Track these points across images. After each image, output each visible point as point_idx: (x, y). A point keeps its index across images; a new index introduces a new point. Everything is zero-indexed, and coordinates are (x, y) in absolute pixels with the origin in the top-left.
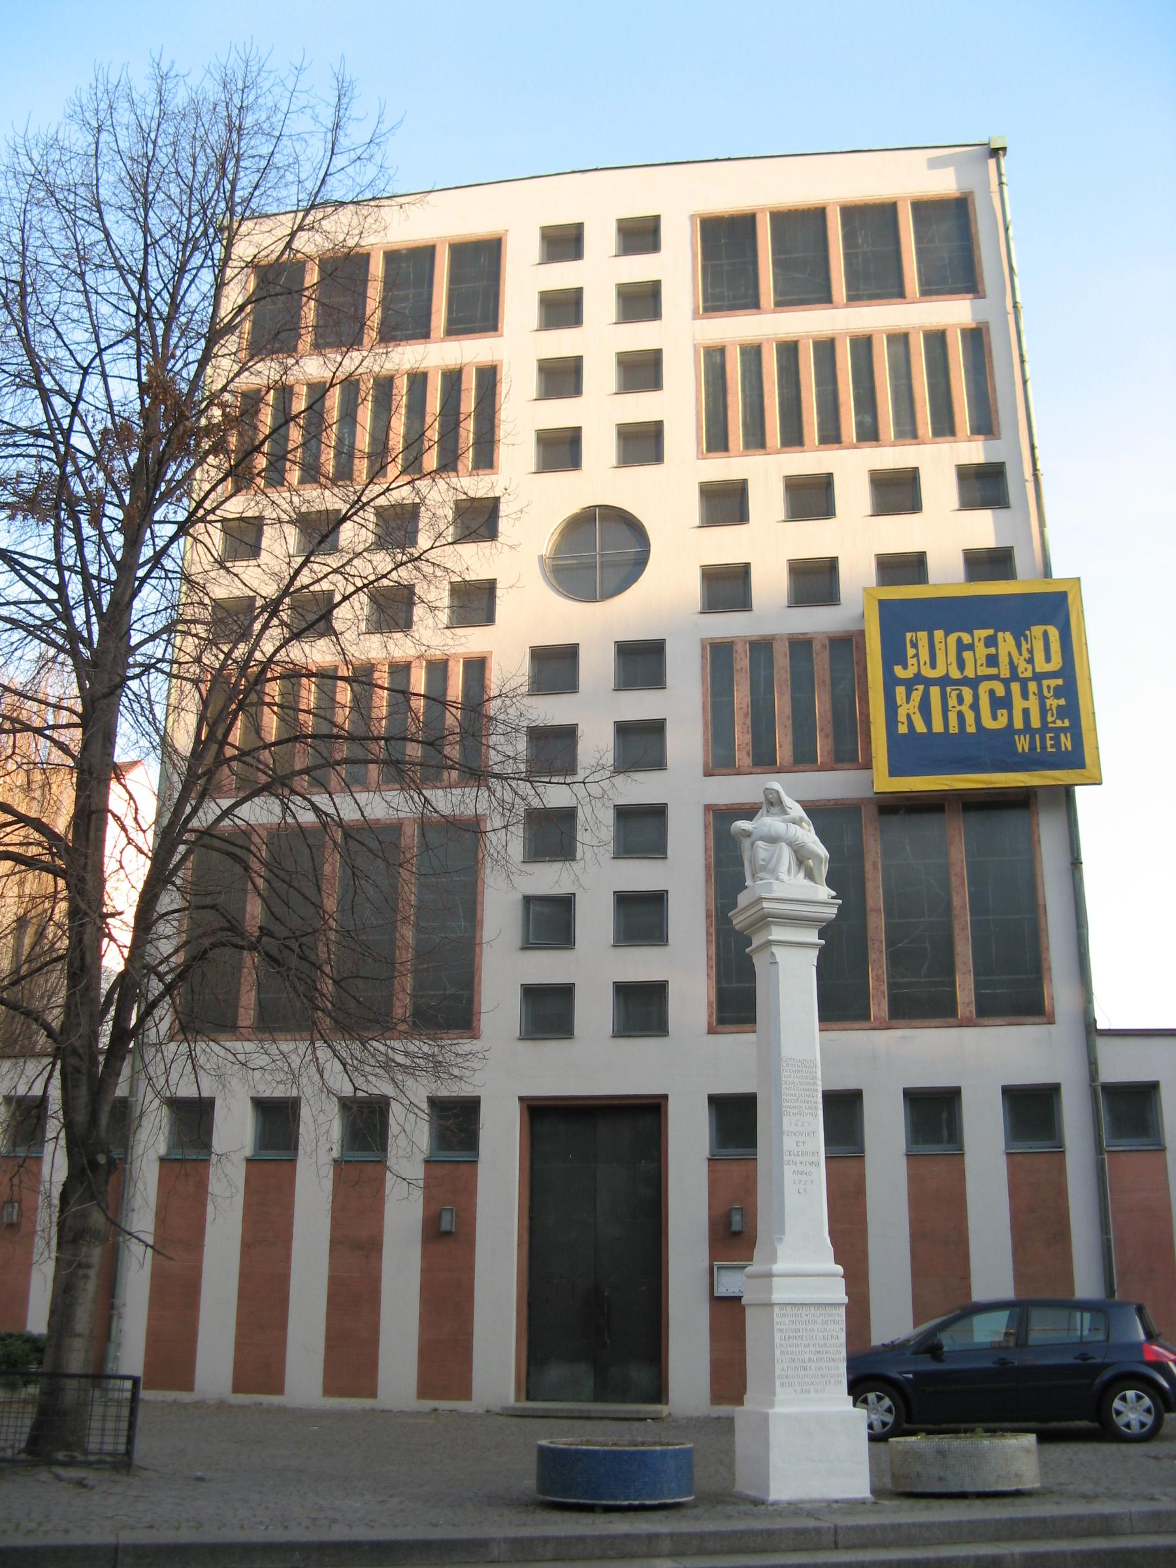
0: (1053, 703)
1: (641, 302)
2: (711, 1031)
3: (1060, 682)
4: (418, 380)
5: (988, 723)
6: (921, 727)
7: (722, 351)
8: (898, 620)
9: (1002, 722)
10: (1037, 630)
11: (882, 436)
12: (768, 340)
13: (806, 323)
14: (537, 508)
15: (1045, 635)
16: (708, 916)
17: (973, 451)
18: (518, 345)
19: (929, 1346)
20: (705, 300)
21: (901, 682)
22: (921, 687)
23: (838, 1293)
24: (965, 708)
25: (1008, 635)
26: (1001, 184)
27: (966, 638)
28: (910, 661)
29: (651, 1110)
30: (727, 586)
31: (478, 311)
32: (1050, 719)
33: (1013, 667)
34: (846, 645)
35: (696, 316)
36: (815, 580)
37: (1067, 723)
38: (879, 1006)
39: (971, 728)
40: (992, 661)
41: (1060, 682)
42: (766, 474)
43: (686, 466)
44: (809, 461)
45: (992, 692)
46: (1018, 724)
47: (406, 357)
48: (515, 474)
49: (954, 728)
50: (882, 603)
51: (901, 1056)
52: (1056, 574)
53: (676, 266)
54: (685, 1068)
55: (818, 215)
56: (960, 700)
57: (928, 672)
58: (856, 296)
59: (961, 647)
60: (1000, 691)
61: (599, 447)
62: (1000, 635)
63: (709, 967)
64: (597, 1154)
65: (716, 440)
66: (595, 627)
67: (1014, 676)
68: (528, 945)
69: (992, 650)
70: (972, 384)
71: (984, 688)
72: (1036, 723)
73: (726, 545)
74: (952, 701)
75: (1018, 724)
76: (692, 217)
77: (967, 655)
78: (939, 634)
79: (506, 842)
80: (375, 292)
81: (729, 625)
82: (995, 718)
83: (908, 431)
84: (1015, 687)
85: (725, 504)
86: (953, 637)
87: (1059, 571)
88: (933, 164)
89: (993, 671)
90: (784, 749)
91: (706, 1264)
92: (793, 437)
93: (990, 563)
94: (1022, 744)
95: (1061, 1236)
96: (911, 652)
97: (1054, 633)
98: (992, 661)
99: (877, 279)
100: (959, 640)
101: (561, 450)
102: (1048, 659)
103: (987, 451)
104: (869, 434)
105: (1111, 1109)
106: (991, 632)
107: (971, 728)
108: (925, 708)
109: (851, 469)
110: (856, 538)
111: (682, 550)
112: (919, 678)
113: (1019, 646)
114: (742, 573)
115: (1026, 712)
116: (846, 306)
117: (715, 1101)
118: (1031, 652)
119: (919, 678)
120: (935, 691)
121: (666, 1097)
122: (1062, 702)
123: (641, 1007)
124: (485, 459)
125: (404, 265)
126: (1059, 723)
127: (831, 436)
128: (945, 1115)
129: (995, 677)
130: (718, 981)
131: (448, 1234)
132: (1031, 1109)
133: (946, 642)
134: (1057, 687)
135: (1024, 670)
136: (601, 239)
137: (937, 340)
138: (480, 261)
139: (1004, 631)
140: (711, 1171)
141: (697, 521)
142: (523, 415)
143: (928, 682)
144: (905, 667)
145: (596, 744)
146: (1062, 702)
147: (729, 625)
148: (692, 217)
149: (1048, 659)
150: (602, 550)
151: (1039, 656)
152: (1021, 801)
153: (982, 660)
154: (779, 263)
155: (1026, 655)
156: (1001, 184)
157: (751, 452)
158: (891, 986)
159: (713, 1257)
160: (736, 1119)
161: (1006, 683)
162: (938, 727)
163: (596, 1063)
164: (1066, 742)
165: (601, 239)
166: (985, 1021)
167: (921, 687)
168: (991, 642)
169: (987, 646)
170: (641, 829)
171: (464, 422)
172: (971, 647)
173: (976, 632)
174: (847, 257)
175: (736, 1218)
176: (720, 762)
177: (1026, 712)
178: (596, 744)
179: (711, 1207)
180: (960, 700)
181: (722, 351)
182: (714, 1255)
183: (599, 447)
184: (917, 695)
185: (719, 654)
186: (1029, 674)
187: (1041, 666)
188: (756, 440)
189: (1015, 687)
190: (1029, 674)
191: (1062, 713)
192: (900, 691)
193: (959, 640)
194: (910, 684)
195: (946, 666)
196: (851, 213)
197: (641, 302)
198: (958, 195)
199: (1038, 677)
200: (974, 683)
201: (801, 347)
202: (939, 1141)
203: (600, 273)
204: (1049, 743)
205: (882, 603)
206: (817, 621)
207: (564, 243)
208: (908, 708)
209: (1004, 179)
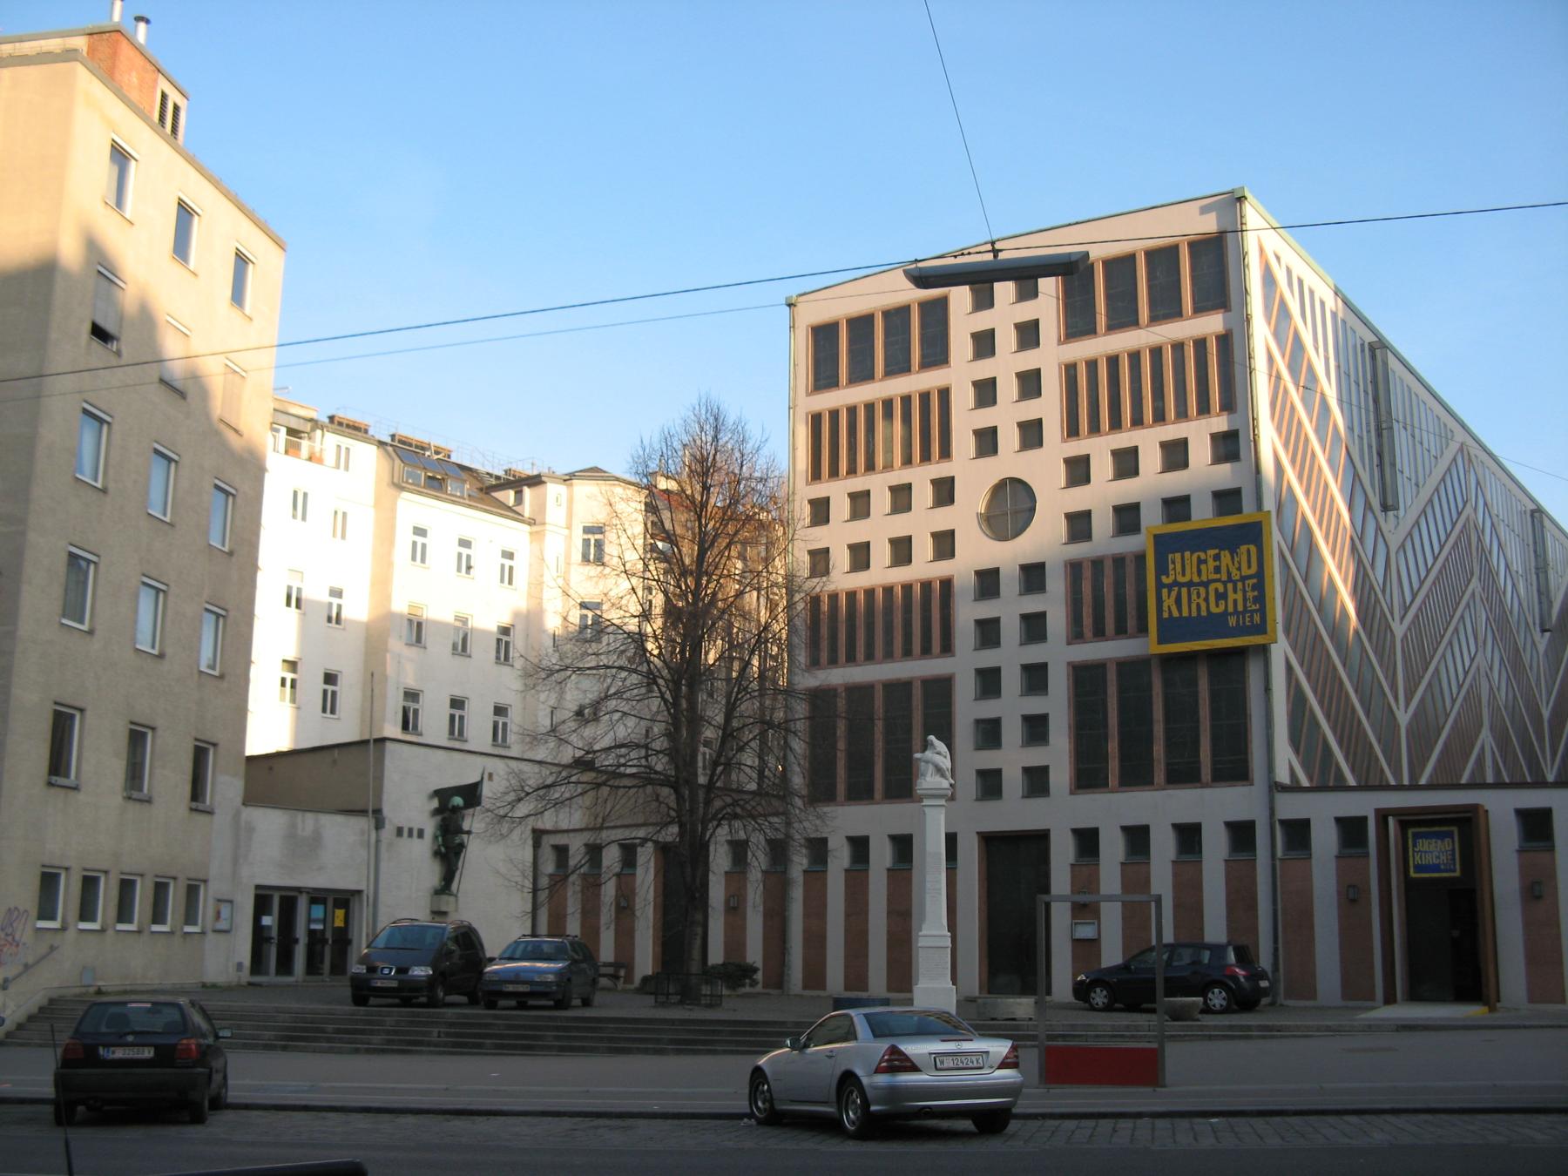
0: (1250, 595)
2: (1072, 793)
5: (1214, 609)
6: (1176, 614)
9: (1221, 609)
10: (1243, 548)
14: (975, 479)
17: (1220, 423)
19: (1125, 967)
20: (1067, 328)
21: (1164, 586)
27: (1203, 556)
29: (1039, 840)
30: (1079, 524)
33: (1229, 574)
36: (1127, 517)
38: (1160, 775)
39: (1204, 613)
40: (1217, 570)
42: (1100, 450)
43: (1056, 447)
46: (1231, 609)
48: (964, 465)
49: (1194, 614)
55: (1130, 258)
56: (1199, 595)
57: (1181, 579)
59: (1200, 562)
60: (1221, 590)
61: (1009, 438)
65: (1073, 431)
66: (1008, 555)
67: (1230, 579)
68: (979, 748)
71: (1212, 587)
72: (1240, 608)
74: (1194, 596)
75: (1231, 609)
77: (1203, 567)
78: (1187, 554)
81: (1081, 550)
84: (1230, 586)
85: (1078, 471)
88: (1204, 210)
93: (1227, 499)
94: (1232, 621)
98: (1217, 570)
103: (1229, 421)
107: (1204, 613)
108: (1178, 601)
109: (1149, 442)
111: (1054, 501)
115: (1235, 601)
119: (1176, 583)
120: (1184, 590)
123: (1037, 781)
124: (946, 453)
132: (1241, 834)
133: (1191, 558)
135: (1236, 575)
142: (965, 419)
143: (1181, 585)
150: (1011, 506)
152: (1241, 653)
153: (1211, 569)
154: (1108, 297)
161: (1225, 583)
162: (1185, 613)
168: (1217, 558)
170: (1035, 677)
171: (928, 427)
172: (1205, 562)
176: (1076, 635)
177: (1235, 601)
180: (1199, 595)
182: (1074, 917)
183: (1009, 438)
185: (1074, 568)
187: (1245, 572)
189: (1230, 586)
192: (1165, 591)
194: (1170, 587)
195: (1190, 575)
199: (1244, 579)
200: (1206, 585)
206: (1129, 544)
208: (1168, 602)
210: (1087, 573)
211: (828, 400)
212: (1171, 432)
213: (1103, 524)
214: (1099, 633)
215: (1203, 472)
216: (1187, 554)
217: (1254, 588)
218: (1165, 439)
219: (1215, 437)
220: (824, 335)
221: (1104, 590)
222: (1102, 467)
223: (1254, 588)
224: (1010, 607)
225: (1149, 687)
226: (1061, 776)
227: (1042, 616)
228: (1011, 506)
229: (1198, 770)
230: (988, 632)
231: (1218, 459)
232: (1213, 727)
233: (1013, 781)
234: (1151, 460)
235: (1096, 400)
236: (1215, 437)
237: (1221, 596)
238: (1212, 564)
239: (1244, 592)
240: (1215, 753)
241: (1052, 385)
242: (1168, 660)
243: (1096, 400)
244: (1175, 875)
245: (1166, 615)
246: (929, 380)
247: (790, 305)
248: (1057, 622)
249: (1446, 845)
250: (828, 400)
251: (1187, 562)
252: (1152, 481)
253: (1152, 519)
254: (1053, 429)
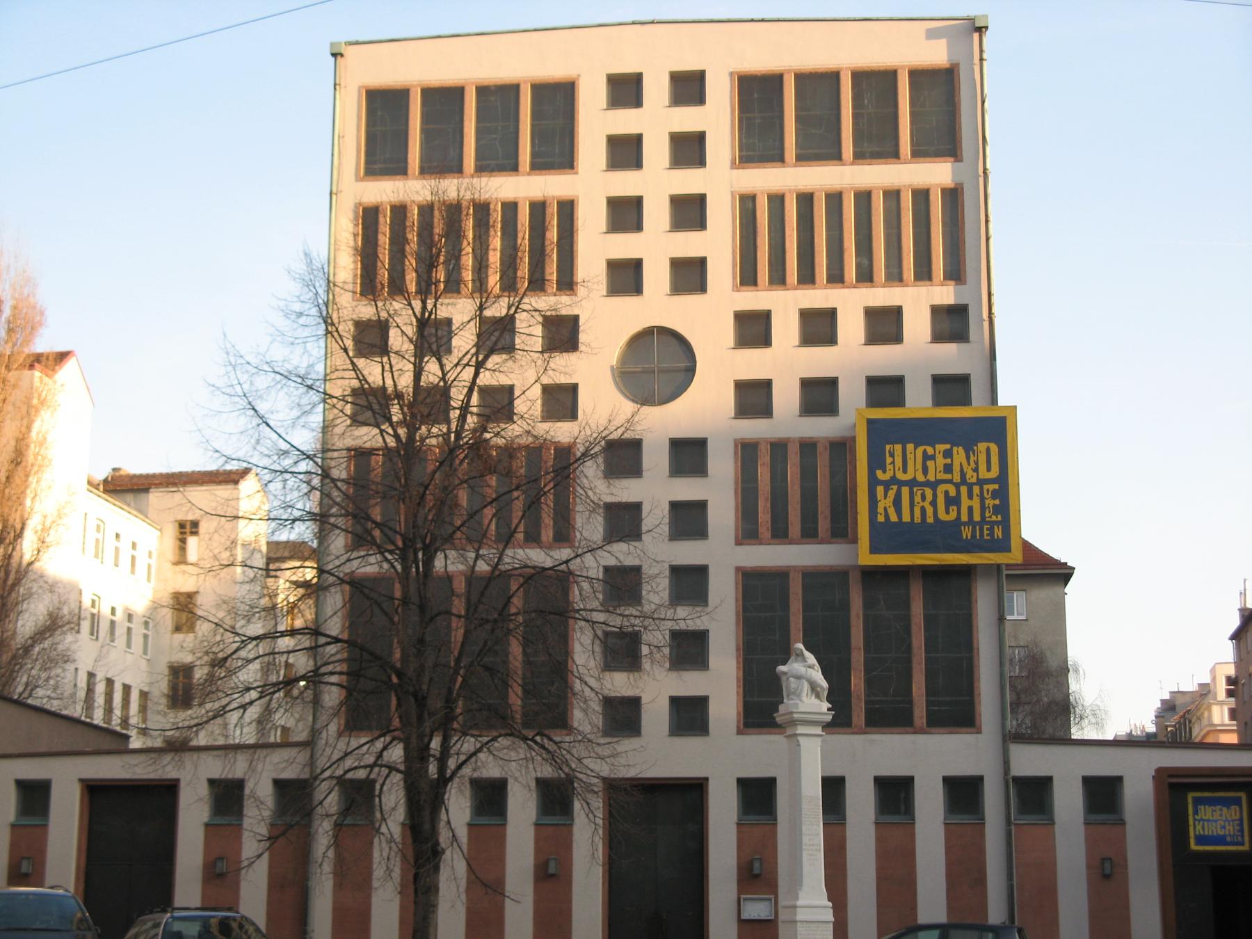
0: (990, 502)
1: (688, 149)
2: (739, 732)
3: (996, 486)
4: (510, 208)
5: (942, 516)
6: (894, 518)
7: (753, 198)
8: (881, 433)
9: (953, 516)
10: (982, 446)
11: (875, 279)
12: (790, 191)
13: (819, 178)
14: (608, 324)
15: (988, 450)
16: (738, 650)
17: (945, 294)
18: (590, 184)
22: (895, 487)
23: (829, 916)
24: (927, 504)
25: (961, 449)
26: (981, 59)
27: (930, 450)
28: (889, 467)
29: (695, 789)
30: (753, 397)
31: (557, 151)
32: (987, 514)
33: (963, 475)
34: (841, 448)
35: (733, 166)
36: (819, 395)
37: (999, 518)
39: (930, 520)
40: (948, 469)
41: (996, 486)
42: (785, 306)
43: (724, 297)
44: (818, 298)
45: (946, 492)
46: (964, 518)
47: (501, 188)
49: (917, 519)
50: (870, 422)
51: (891, 752)
52: (1001, 403)
53: (717, 118)
54: (722, 758)
56: (923, 498)
57: (901, 476)
58: (860, 156)
59: (926, 457)
60: (953, 493)
61: (657, 276)
62: (955, 449)
63: (738, 687)
64: (661, 817)
65: (748, 277)
69: (949, 461)
70: (948, 236)
71: (941, 489)
72: (977, 518)
73: (753, 363)
74: (918, 498)
75: (964, 518)
76: (731, 74)
77: (930, 464)
81: (755, 428)
82: (947, 512)
83: (895, 277)
84: (964, 489)
85: (753, 329)
86: (920, 450)
87: (1005, 398)
88: (931, 35)
89: (948, 476)
90: (795, 527)
91: (735, 896)
92: (807, 278)
93: (951, 387)
94: (966, 533)
95: (980, 881)
96: (889, 460)
97: (994, 448)
98: (948, 469)
99: (878, 143)
100: (925, 452)
101: (626, 277)
102: (989, 470)
104: (866, 276)
105: (1020, 795)
106: (948, 446)
107: (930, 520)
109: (851, 305)
111: (720, 365)
112: (894, 480)
113: (968, 458)
114: (765, 386)
115: (970, 509)
116: (853, 164)
117: (742, 783)
118: (976, 463)
119: (894, 480)
121: (707, 779)
122: (997, 502)
125: (493, 98)
126: (994, 518)
127: (837, 277)
128: (903, 795)
129: (950, 482)
130: (744, 697)
131: (552, 875)
132: (963, 793)
133: (915, 453)
134: (994, 490)
135: (971, 477)
136: (656, 90)
137: (922, 196)
138: (557, 99)
139: (958, 445)
140: (739, 832)
141: (732, 344)
142: (596, 247)
143: (901, 484)
144: (884, 472)
145: (656, 517)
146: (997, 502)
147: (755, 428)
148: (731, 74)
149: (989, 470)
150: (659, 362)
151: (983, 467)
152: (966, 573)
155: (973, 465)
156: (981, 59)
157: (774, 287)
158: (867, 703)
159: (740, 892)
160: (758, 796)
161: (957, 486)
162: (906, 518)
163: (656, 754)
164: (998, 532)
165: (656, 90)
166: (933, 730)
167: (895, 487)
168: (948, 454)
169: (945, 457)
171: (543, 247)
172: (933, 458)
173: (938, 446)
174: (855, 116)
175: (757, 865)
176: (748, 533)
177: (970, 509)
178: (656, 517)
179: (739, 857)
180: (923, 498)
181: (753, 198)
182: (741, 890)
183: (657, 276)
185: (747, 451)
186: (974, 480)
187: (984, 474)
188: (778, 278)
189: (964, 489)
190: (974, 480)
191: (996, 510)
192: (880, 489)
193: (925, 452)
194: (887, 485)
196: (860, 77)
197: (688, 149)
198: (948, 66)
199: (981, 482)
200: (934, 485)
201: (815, 198)
202: (897, 812)
203: (656, 120)
204: (986, 532)
205: (870, 422)
206: (821, 428)
207: (626, 90)
208: (885, 503)
209: (985, 56)
210: (764, 458)
211: (385, 191)
212: (882, 296)
213: (786, 398)
214: (780, 534)
215: (918, 352)
216: (910, 447)
217: (995, 495)
218: (872, 304)
219: (936, 311)
220: (384, 106)
221: (796, 482)
222: (786, 329)
223: (995, 495)
224: (655, 490)
225: (845, 606)
226: (725, 705)
227: (701, 506)
228: (659, 362)
229: (910, 712)
230: (624, 522)
231: (938, 336)
232: (928, 661)
233: (656, 715)
234: (851, 327)
235: (779, 244)
236: (936, 311)
237: (952, 501)
238: (941, 461)
239: (982, 499)
240: (930, 691)
241: (722, 216)
242: (870, 574)
243: (779, 244)
244: (880, 840)
245: (881, 519)
246: (550, 186)
247: (334, 55)
248: (723, 514)
249: (1232, 813)
250: (385, 191)
251: (910, 456)
252: (851, 357)
253: (852, 397)
254: (721, 270)
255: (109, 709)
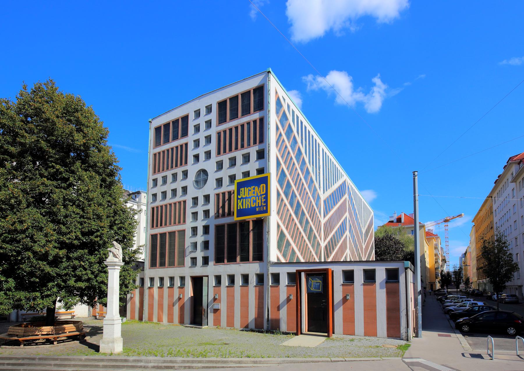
6: (242, 208)
9: (254, 205)
10: (262, 185)
33: (257, 194)
40: (254, 193)
42: (225, 158)
43: (214, 158)
46: (257, 206)
57: (243, 196)
59: (249, 190)
71: (252, 198)
79: (212, 213)
80: (226, 255)
85: (220, 165)
94: (257, 209)
97: (264, 185)
98: (254, 193)
107: (249, 207)
109: (238, 155)
110: (238, 171)
119: (242, 198)
120: (244, 200)
161: (256, 197)
162: (244, 208)
168: (254, 189)
184: (241, 201)
189: (257, 198)
191: (265, 202)
194: (240, 199)
195: (246, 195)
200: (250, 198)
238: (252, 191)
245: (239, 208)
255: (303, 249)
